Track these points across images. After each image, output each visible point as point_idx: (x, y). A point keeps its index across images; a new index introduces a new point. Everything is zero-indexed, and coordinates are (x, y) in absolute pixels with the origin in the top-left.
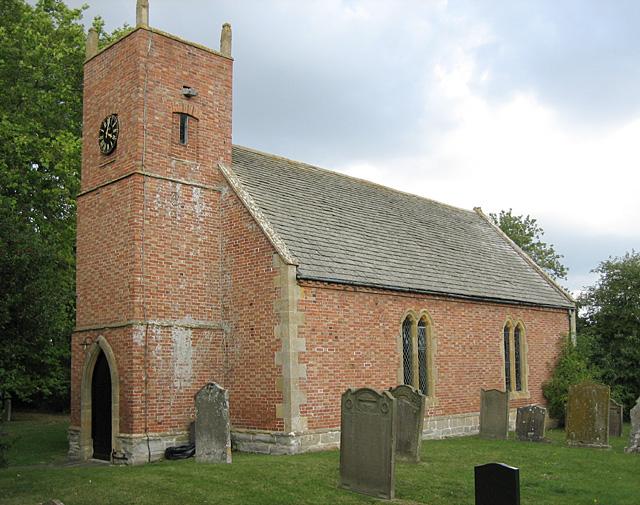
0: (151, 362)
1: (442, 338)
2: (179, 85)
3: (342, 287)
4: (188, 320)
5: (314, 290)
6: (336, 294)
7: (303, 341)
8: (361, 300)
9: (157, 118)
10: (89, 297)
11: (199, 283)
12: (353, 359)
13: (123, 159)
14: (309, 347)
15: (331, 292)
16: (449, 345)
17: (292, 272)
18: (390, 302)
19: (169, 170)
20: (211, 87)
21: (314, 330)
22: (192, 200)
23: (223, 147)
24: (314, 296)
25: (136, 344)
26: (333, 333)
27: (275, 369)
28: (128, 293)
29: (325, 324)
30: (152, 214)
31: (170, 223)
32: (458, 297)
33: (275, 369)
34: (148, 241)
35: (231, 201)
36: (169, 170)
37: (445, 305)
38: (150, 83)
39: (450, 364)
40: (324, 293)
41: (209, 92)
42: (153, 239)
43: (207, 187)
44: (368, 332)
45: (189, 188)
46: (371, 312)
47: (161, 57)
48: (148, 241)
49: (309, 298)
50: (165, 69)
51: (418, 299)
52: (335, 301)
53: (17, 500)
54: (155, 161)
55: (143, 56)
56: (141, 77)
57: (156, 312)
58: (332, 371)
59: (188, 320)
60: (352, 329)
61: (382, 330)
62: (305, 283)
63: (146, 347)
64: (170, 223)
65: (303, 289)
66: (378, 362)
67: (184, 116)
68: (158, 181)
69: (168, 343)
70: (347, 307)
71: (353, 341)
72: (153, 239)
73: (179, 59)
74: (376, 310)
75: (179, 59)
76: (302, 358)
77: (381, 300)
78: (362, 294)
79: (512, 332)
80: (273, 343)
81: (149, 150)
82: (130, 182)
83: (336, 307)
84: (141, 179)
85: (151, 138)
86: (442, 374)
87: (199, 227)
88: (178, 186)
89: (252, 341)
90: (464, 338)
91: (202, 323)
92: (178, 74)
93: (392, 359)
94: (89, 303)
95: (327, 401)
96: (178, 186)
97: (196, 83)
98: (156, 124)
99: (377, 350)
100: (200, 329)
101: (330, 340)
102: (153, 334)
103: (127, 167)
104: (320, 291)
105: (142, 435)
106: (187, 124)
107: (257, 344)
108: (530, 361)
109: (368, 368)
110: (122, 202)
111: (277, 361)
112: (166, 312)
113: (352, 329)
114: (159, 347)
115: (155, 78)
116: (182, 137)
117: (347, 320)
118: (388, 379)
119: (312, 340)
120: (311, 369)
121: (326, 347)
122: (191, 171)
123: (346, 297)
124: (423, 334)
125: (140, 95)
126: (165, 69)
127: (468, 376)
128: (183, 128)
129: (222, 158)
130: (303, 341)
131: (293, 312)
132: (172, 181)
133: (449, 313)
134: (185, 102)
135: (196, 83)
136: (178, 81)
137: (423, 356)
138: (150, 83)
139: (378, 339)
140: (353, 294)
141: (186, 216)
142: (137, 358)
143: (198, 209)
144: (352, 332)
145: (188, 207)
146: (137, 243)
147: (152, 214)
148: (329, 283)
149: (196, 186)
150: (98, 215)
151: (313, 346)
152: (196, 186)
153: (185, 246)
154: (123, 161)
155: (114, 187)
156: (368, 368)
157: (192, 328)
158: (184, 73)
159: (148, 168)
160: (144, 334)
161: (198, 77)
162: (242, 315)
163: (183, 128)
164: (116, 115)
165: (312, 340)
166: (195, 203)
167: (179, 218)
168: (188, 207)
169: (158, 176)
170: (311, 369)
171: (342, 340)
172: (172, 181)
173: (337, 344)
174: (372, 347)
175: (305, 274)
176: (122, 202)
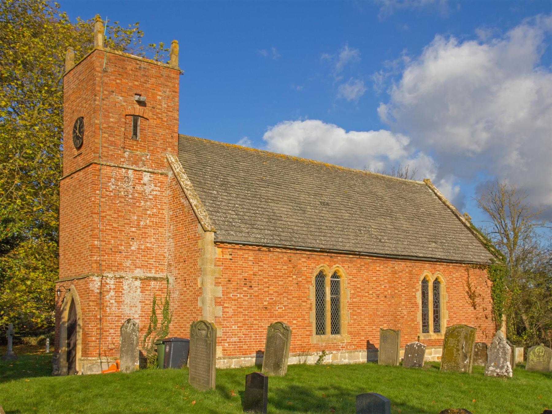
0: (105, 304)
1: (355, 288)
2: (131, 93)
3: (257, 248)
4: (139, 273)
5: (229, 250)
6: (251, 253)
7: (220, 288)
8: (275, 257)
9: (112, 120)
10: (67, 257)
11: (148, 245)
12: (266, 303)
13: (87, 152)
14: (225, 293)
15: (247, 252)
16: (363, 293)
17: (210, 237)
18: (304, 260)
19: (122, 160)
20: (160, 93)
21: (229, 281)
22: (142, 182)
23: (170, 140)
24: (231, 255)
25: (92, 291)
26: (247, 282)
27: (199, 310)
28: (89, 252)
29: (241, 277)
30: (108, 193)
31: (123, 200)
32: (371, 255)
33: (199, 310)
34: (103, 214)
35: (174, 183)
36: (122, 160)
37: (359, 261)
38: (106, 93)
39: (363, 309)
40: (240, 252)
41: (159, 97)
42: (108, 213)
43: (156, 171)
44: (281, 283)
45: (140, 173)
46: (285, 267)
47: (116, 71)
48: (103, 214)
49: (225, 257)
50: (118, 81)
51: (331, 257)
52: (251, 258)
53: (296, 412)
54: (110, 153)
55: (99, 72)
56: (98, 88)
57: (109, 267)
58: (246, 312)
59: (139, 273)
60: (266, 280)
61: (295, 281)
62: (222, 245)
63: (101, 293)
64: (123, 200)
65: (221, 250)
66: (290, 306)
67: (136, 118)
68: (113, 168)
69: (118, 290)
70: (261, 264)
71: (266, 289)
72: (108, 213)
73: (130, 72)
74: (290, 265)
75: (130, 72)
76: (218, 302)
77: (294, 258)
78: (277, 253)
79: (431, 285)
80: (198, 291)
81: (105, 145)
82: (90, 169)
83: (251, 263)
84: (98, 167)
85: (106, 135)
86: (355, 317)
87: (148, 203)
88: (130, 172)
89: (185, 289)
90: (378, 289)
91: (149, 275)
92: (130, 84)
93: (304, 304)
94: (67, 261)
95: (240, 335)
96: (130, 172)
97: (147, 90)
98: (111, 125)
99: (290, 297)
100: (149, 279)
101: (245, 289)
102: (107, 284)
103: (91, 157)
104: (236, 251)
105: (96, 358)
106: (139, 123)
107: (188, 291)
108: (449, 308)
109: (280, 310)
110: (85, 185)
111: (200, 304)
112: (120, 267)
113: (266, 280)
114: (112, 293)
115: (110, 89)
116: (135, 134)
117: (260, 273)
118: (300, 319)
119: (228, 288)
120: (226, 310)
121: (241, 293)
122: (141, 160)
123: (261, 255)
124: (336, 287)
125: (97, 103)
126: (118, 81)
127: (382, 319)
128: (135, 126)
129: (169, 149)
130: (220, 288)
131: (210, 267)
132: (125, 168)
133: (363, 268)
134: (137, 106)
135: (147, 90)
136: (130, 90)
137: (335, 302)
138: (106, 93)
139: (292, 288)
140: (268, 253)
141: (136, 195)
142: (93, 301)
143: (147, 189)
144: (266, 283)
145: (138, 188)
146: (94, 216)
147: (108, 193)
148: (244, 245)
149: (145, 171)
150: (72, 194)
151: (229, 293)
152: (145, 171)
153: (136, 218)
154: (88, 154)
155: (81, 173)
156: (280, 310)
157: (141, 279)
158: (136, 83)
159: (104, 158)
160: (99, 284)
161: (148, 85)
162: (179, 269)
163: (135, 126)
164: (83, 118)
165: (228, 288)
166: (145, 185)
167: (130, 196)
168: (138, 188)
169: (112, 164)
170: (226, 310)
171: (256, 289)
172: (125, 168)
173: (252, 291)
174: (285, 295)
175: (221, 238)
176: (85, 185)
